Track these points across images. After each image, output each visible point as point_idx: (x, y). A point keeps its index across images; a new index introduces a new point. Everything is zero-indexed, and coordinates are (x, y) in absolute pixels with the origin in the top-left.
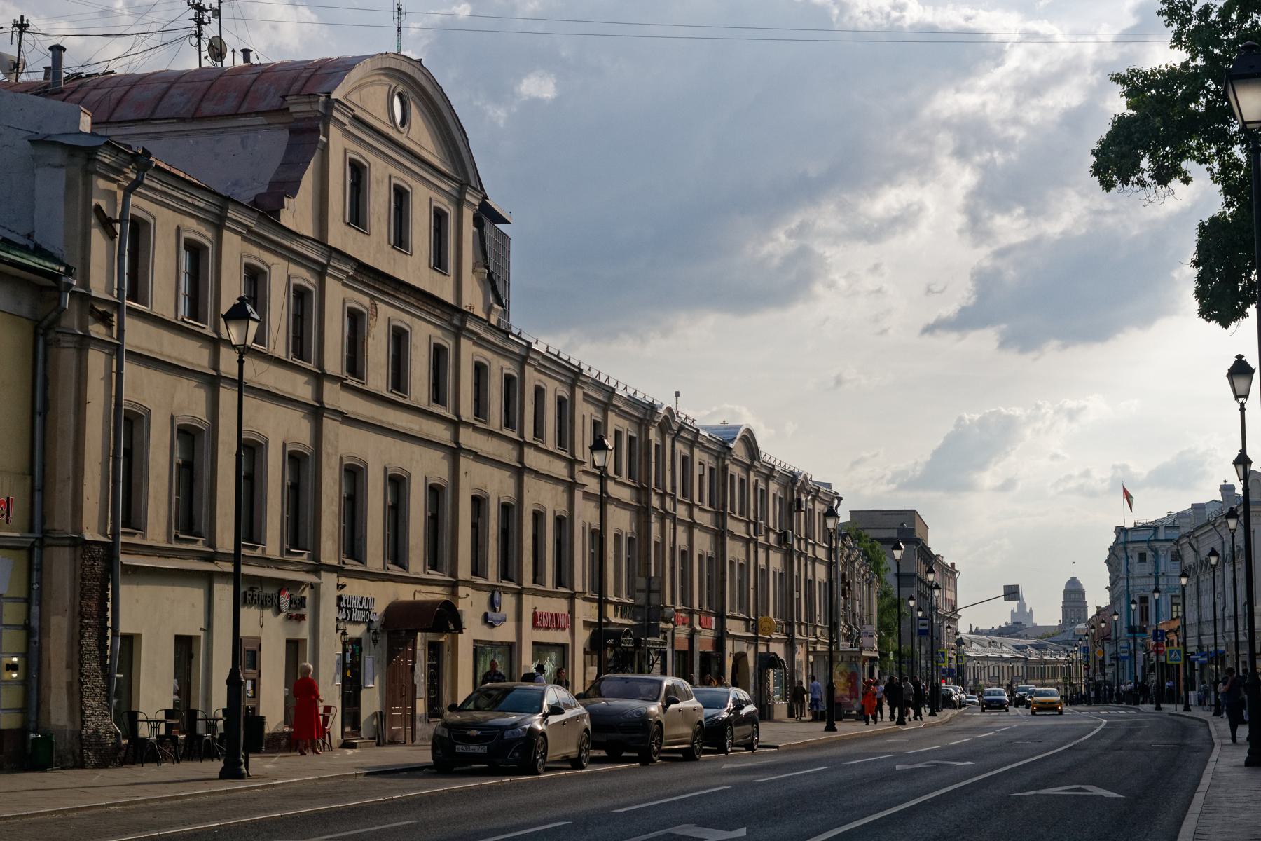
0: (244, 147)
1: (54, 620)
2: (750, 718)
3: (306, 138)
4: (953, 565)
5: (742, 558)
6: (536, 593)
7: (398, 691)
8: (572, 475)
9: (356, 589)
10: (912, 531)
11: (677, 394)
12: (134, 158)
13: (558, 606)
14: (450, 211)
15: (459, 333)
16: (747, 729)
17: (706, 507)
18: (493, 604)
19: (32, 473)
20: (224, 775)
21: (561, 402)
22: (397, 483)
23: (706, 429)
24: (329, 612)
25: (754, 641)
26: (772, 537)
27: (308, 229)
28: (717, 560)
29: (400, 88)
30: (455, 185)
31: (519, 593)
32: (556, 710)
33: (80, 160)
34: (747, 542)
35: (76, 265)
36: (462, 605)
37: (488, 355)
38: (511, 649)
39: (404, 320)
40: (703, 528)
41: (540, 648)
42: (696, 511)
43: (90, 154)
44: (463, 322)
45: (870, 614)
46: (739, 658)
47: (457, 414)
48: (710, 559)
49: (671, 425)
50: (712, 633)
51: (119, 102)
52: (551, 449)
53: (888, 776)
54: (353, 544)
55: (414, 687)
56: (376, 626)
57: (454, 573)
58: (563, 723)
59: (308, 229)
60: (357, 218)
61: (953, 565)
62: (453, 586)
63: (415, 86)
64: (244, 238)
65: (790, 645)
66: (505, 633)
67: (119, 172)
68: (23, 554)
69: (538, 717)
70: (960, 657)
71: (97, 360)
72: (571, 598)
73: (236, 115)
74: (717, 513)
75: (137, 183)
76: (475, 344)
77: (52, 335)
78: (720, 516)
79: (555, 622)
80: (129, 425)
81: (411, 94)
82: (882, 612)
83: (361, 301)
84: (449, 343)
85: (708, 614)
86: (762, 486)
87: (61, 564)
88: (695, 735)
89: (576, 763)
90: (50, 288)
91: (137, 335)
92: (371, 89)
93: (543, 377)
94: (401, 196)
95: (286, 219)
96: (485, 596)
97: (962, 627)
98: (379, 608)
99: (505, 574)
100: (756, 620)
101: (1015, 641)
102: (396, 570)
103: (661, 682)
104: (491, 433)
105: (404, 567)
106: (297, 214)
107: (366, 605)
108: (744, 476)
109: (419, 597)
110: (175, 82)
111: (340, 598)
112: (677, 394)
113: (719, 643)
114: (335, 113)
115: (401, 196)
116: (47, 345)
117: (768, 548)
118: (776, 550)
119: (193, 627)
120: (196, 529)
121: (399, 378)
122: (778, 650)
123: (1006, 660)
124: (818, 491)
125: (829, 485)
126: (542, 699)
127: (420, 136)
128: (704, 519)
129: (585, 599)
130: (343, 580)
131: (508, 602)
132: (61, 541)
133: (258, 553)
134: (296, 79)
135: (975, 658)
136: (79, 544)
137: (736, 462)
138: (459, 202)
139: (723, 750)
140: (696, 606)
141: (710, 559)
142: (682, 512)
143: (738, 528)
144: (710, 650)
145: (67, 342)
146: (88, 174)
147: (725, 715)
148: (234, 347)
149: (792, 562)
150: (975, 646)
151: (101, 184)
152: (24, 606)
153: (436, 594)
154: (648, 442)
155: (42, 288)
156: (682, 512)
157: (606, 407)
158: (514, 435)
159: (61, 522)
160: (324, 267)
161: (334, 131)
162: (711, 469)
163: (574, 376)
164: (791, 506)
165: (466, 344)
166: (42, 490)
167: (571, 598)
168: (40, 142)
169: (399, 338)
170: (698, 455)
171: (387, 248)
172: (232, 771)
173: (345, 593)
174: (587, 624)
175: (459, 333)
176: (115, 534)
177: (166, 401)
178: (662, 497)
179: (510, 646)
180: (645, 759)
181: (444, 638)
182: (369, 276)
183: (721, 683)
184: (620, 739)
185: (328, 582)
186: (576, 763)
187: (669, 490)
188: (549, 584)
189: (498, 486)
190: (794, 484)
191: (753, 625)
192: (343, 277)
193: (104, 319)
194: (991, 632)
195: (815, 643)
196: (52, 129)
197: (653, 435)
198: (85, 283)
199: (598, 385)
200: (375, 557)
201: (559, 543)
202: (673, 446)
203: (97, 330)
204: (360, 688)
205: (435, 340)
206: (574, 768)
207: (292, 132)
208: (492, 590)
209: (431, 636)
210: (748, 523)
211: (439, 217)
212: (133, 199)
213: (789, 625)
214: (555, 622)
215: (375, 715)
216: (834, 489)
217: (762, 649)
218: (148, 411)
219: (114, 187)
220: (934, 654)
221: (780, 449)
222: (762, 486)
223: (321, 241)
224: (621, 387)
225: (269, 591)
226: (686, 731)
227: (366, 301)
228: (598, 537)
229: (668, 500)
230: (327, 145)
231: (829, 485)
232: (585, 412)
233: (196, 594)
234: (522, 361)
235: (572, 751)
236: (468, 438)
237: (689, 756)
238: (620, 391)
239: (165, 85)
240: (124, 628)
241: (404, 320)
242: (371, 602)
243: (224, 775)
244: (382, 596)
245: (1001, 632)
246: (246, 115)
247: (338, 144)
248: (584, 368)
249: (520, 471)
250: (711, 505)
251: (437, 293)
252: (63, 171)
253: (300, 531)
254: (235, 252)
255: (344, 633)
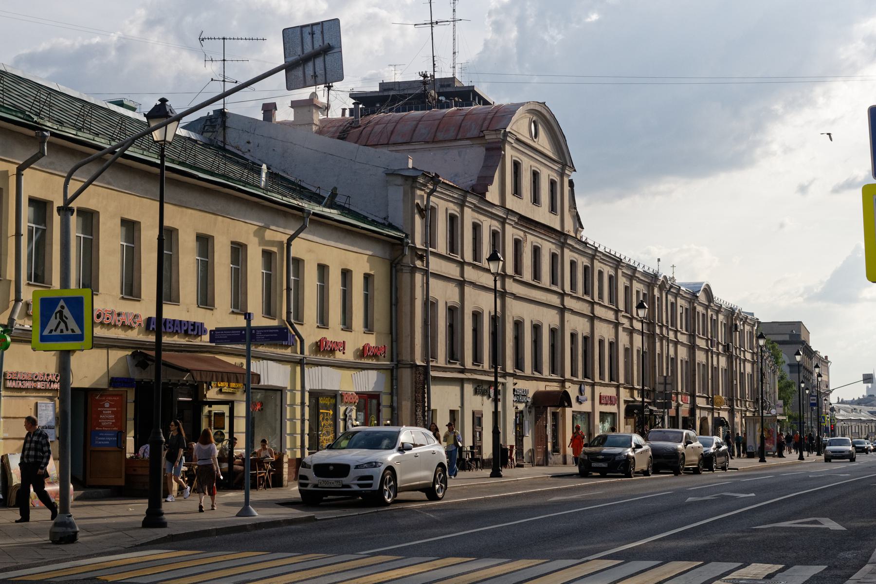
0: (460, 156)
1: (404, 403)
2: (724, 453)
3: (495, 151)
4: (826, 357)
5: (704, 361)
6: (601, 385)
7: (540, 438)
8: (617, 319)
9: (522, 385)
10: (799, 335)
11: (659, 260)
12: (432, 178)
13: (611, 392)
14: (557, 179)
15: (563, 246)
16: (723, 459)
17: (684, 332)
18: (581, 392)
19: (391, 333)
20: (492, 476)
21: (610, 277)
22: (537, 328)
23: (685, 285)
24: (510, 397)
25: (712, 410)
26: (721, 347)
27: (497, 202)
28: (691, 361)
29: (534, 118)
30: (560, 166)
31: (593, 385)
32: (638, 446)
33: (409, 182)
34: (707, 351)
35: (409, 232)
36: (569, 390)
37: (576, 255)
38: (589, 416)
39: (538, 241)
40: (683, 344)
41: (603, 415)
42: (679, 334)
43: (414, 179)
44: (566, 240)
45: (775, 392)
46: (704, 420)
47: (563, 289)
48: (687, 362)
49: (668, 287)
50: (688, 406)
51: (392, 132)
52: (606, 304)
53: (807, 479)
54: (519, 363)
55: (547, 436)
56: (529, 404)
57: (563, 376)
58: (641, 453)
59: (497, 202)
60: (517, 192)
61: (826, 357)
62: (563, 382)
63: (543, 118)
64: (473, 210)
65: (732, 412)
66: (586, 407)
67: (425, 186)
68: (389, 372)
69: (629, 450)
70: (833, 419)
71: (418, 277)
72: (618, 387)
73: (456, 140)
74: (690, 335)
75: (433, 191)
76: (571, 251)
77: (399, 267)
78: (692, 336)
79: (610, 401)
80: (430, 305)
81: (539, 120)
82: (780, 389)
83: (519, 234)
84: (558, 252)
85: (686, 394)
86: (714, 317)
87: (406, 376)
88: (700, 460)
89: (646, 473)
90: (398, 244)
91: (435, 264)
92: (521, 121)
93: (602, 265)
94: (535, 175)
95: (489, 197)
96: (577, 387)
97: (833, 399)
98: (531, 395)
99: (586, 376)
100: (712, 398)
101: (870, 409)
102: (537, 375)
103: (682, 433)
104: (578, 298)
105: (541, 373)
106: (492, 195)
107: (525, 394)
108: (704, 312)
109: (548, 389)
110: (420, 121)
111: (514, 390)
112: (659, 260)
113: (692, 412)
114: (508, 139)
115: (535, 175)
116: (397, 271)
117: (718, 354)
118: (723, 355)
119: (456, 406)
120: (455, 357)
121: (536, 275)
122: (725, 415)
123: (864, 421)
124: (747, 318)
125: (752, 314)
126: (631, 441)
127: (543, 143)
128: (683, 338)
129: (625, 388)
130: (515, 381)
131: (587, 390)
132: (406, 366)
133: (480, 368)
134: (485, 119)
135: (842, 420)
136: (414, 366)
137: (701, 304)
138: (562, 175)
139: (711, 469)
140: (680, 390)
141: (687, 362)
142: (671, 336)
143: (701, 343)
144: (687, 415)
145: (406, 270)
146: (413, 188)
147: (712, 451)
148: (492, 274)
149: (732, 362)
150: (842, 412)
151: (419, 192)
152: (389, 396)
153: (554, 387)
154: (654, 296)
155: (393, 244)
156: (671, 336)
157: (631, 278)
158: (589, 299)
159: (406, 357)
160: (505, 219)
161: (508, 147)
162: (686, 309)
163: (617, 263)
164: (731, 328)
165: (566, 251)
166: (396, 341)
167: (618, 387)
168: (391, 174)
169: (536, 251)
170: (680, 302)
171: (531, 204)
172: (496, 474)
173: (516, 387)
174: (626, 402)
175: (563, 246)
176: (428, 362)
177: (444, 294)
178: (661, 327)
179: (588, 414)
180: (677, 473)
181: (559, 410)
182: (526, 222)
183: (708, 435)
184: (666, 462)
185: (510, 381)
186: (646, 473)
187: (664, 323)
188: (607, 381)
189: (486, 303)
190: (733, 315)
191: (711, 401)
192: (513, 223)
193: (421, 258)
194: (852, 402)
195: (746, 411)
196: (395, 167)
197: (656, 292)
198: (413, 242)
199: (629, 266)
200: (528, 370)
201: (553, 347)
202: (667, 297)
203: (418, 263)
204: (523, 436)
205: (553, 251)
206: (645, 475)
207: (487, 149)
208: (580, 384)
209: (553, 409)
210: (707, 340)
211: (553, 183)
212: (432, 198)
213: (731, 400)
214: (610, 401)
215: (530, 450)
216: (756, 316)
217: (716, 415)
218: (437, 301)
219: (422, 193)
220: (819, 418)
221: (724, 296)
222: (714, 317)
223: (503, 206)
224: (641, 266)
225: (485, 387)
226: (695, 458)
227: (522, 234)
228: (628, 351)
229: (664, 329)
230: (504, 155)
231: (752, 314)
232: (622, 282)
233: (456, 389)
234: (592, 258)
235: (644, 467)
236: (569, 303)
237: (696, 471)
238: (640, 269)
239: (415, 123)
240: (432, 407)
241: (538, 241)
242: (527, 391)
243: (492, 476)
244: (532, 388)
245: (860, 402)
246: (461, 139)
247: (510, 154)
248: (622, 258)
249: (592, 318)
250: (687, 330)
251: (552, 226)
252: (402, 188)
253: (497, 358)
254: (470, 216)
255: (517, 408)
